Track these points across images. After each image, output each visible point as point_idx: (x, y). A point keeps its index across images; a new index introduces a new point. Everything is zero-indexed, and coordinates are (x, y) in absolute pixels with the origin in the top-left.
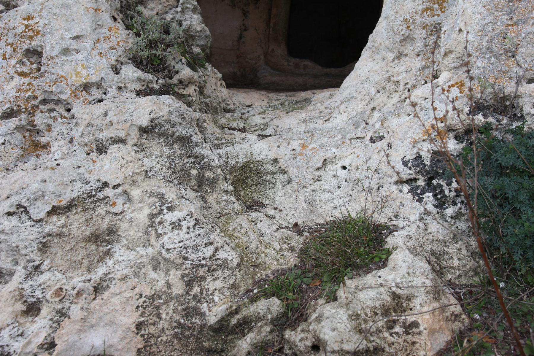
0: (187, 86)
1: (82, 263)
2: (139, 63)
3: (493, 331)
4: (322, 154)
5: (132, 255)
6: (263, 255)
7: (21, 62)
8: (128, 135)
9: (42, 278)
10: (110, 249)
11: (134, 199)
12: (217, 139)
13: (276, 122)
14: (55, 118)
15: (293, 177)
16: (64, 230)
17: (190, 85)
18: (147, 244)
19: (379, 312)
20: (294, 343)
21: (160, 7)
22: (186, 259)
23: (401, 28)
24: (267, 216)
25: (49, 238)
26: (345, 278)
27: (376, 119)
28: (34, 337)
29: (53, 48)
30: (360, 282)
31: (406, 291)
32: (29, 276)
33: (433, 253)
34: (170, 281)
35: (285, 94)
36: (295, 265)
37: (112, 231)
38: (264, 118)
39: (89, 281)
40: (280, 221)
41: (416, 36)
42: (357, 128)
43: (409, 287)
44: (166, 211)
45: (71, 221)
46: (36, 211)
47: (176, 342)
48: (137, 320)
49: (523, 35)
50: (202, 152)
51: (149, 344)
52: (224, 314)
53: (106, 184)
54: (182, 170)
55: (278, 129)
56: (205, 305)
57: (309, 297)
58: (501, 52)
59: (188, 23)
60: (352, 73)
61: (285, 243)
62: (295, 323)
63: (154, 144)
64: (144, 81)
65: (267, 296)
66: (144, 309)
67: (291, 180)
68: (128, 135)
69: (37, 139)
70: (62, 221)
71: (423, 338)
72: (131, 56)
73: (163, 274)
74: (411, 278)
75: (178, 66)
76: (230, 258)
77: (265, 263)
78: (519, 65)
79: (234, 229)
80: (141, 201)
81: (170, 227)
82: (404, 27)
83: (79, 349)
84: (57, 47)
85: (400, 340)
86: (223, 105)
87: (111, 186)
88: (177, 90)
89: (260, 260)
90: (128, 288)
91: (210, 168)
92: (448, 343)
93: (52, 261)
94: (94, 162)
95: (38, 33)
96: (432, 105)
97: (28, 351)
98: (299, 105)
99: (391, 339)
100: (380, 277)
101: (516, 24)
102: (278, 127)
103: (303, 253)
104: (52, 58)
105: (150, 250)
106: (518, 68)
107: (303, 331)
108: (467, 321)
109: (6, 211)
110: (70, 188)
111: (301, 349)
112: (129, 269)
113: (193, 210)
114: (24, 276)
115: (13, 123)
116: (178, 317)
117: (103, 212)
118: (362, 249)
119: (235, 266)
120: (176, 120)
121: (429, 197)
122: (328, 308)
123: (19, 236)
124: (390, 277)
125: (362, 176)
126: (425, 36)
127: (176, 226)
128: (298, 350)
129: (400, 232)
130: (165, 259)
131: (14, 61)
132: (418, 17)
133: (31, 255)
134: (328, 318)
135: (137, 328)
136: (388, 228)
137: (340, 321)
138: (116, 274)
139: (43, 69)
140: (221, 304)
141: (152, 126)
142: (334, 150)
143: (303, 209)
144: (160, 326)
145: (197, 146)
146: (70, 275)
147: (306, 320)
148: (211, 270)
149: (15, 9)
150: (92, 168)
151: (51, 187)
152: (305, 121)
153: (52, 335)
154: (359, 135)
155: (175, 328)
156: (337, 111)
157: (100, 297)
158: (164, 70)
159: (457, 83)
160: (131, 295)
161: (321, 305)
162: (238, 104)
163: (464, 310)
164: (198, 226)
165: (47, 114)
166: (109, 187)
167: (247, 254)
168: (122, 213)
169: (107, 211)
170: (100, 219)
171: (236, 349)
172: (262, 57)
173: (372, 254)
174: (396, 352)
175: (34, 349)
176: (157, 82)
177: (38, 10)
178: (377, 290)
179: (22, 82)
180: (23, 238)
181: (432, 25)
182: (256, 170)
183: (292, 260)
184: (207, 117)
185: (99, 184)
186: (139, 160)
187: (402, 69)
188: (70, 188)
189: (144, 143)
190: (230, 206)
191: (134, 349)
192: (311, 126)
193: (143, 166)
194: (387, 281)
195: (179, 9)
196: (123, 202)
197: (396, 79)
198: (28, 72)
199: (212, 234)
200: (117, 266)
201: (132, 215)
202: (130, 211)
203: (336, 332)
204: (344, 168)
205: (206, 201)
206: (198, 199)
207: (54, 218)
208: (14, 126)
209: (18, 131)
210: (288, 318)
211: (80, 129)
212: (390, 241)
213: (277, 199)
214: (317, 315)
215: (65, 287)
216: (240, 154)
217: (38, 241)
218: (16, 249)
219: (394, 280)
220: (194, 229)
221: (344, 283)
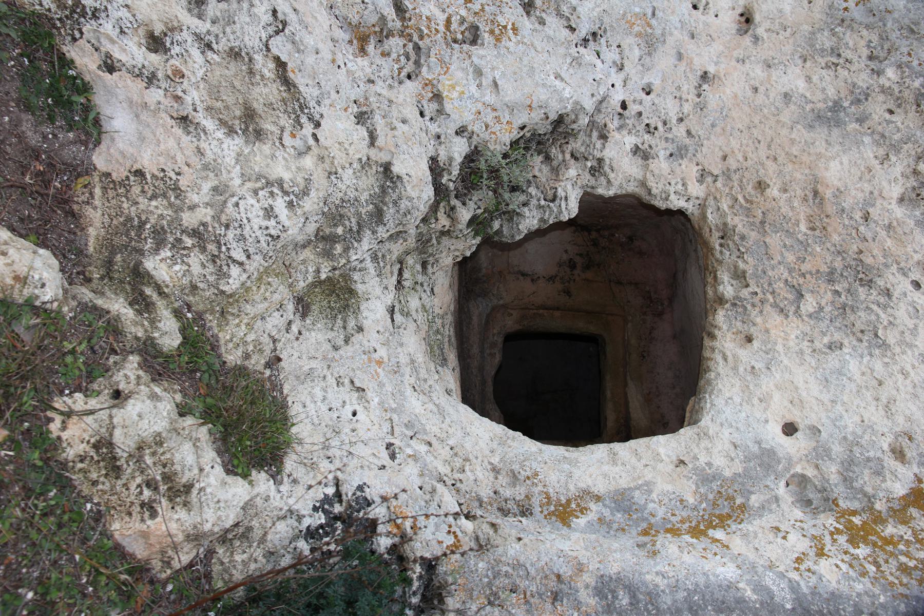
0: (449, 216)
1: (217, 100)
2: (471, 158)
3: (152, 608)
4: (370, 386)
5: (230, 160)
6: (237, 321)
7: (463, 21)
8: (381, 149)
9: (195, 53)
10: (236, 133)
11: (301, 160)
12: (383, 256)
13: (412, 326)
14: (398, 61)
15: (341, 352)
16: (258, 77)
17: (449, 219)
18: (245, 178)
19: (166, 470)
20: (123, 368)
21: (544, 180)
22: (227, 227)
23: (528, 469)
24: (290, 323)
25: (246, 59)
26: (210, 425)
27: (417, 448)
28: (120, 47)
29: (482, 57)
30: (204, 444)
31: (195, 500)
32: (198, 37)
33: (249, 529)
34: (198, 209)
35: (452, 333)
36: (225, 362)
37: (259, 134)
38: (417, 311)
39: (195, 110)
40: (283, 339)
41: (518, 488)
42: (406, 425)
43: (201, 503)
44: (287, 199)
45: (270, 85)
46: (280, 44)
47: (121, 220)
48: (146, 170)
49: (513, 611)
50: (365, 239)
51: (118, 187)
52: (157, 279)
53: (318, 125)
54: (341, 215)
55: (401, 330)
56: (169, 254)
57: (184, 382)
58: (494, 589)
59: (527, 214)
60: (477, 415)
61: (255, 347)
62: (149, 367)
63: (372, 180)
64: (450, 165)
65: (183, 330)
66: (162, 179)
67: (337, 350)
68: (381, 149)
69: (372, 40)
70: (268, 74)
71: (137, 524)
72: (479, 149)
73: (206, 200)
74: (212, 505)
75: (471, 205)
76: (231, 281)
77: (227, 325)
78: (479, 610)
79: (269, 284)
80: (299, 168)
81: (266, 206)
82: (529, 473)
83: (108, 101)
84: (483, 63)
85: (133, 497)
86: (431, 260)
87: (315, 131)
88: (442, 205)
89: (230, 318)
90: (188, 157)
91: (346, 250)
92: (133, 556)
93: (218, 64)
94: (346, 110)
95: (498, 40)
96: (432, 514)
97: (102, 40)
98: (437, 352)
99: (133, 486)
100: (212, 467)
101: (527, 602)
102: (405, 329)
103: (241, 371)
104: (470, 57)
105: (237, 182)
106: (476, 609)
107: (139, 377)
108: (164, 576)
109: (277, 8)
110: (310, 83)
111: (115, 377)
112: (213, 157)
113: (290, 232)
114: (198, 31)
115: (390, 12)
116: (153, 221)
117: (282, 122)
118: (248, 443)
119: (221, 288)
120: (403, 206)
121: (320, 519)
122: (168, 407)
123: (248, 24)
124: (212, 480)
125: (343, 437)
126: (517, 498)
127: (269, 213)
128: (114, 374)
129: (273, 487)
130: (225, 202)
131: (463, 12)
132: (540, 488)
133: (224, 40)
134: (155, 408)
135: (136, 171)
136: (279, 472)
137: (152, 423)
138: (205, 141)
139: (456, 46)
140: (171, 274)
141: (392, 178)
142: (376, 400)
143: (301, 367)
144: (140, 199)
145: (373, 233)
146: (202, 86)
147: (153, 380)
148: (214, 259)
149: (524, 14)
150: (338, 107)
151: (310, 60)
152: (413, 362)
153: (124, 69)
154: (396, 428)
155: (139, 218)
156: (427, 401)
157: (174, 124)
158: (466, 188)
159: (459, 541)
160: (179, 161)
161: (174, 398)
162: (434, 278)
163: (177, 571)
164: (270, 239)
165: (402, 51)
166: (314, 128)
167: (237, 301)
168: (283, 145)
169: (284, 127)
170: (273, 120)
171: (113, 296)
172: (501, 302)
173: (243, 455)
174: (116, 494)
175: (104, 47)
176: (450, 180)
177: (525, 40)
178: (195, 465)
179: (439, 22)
180: (245, 30)
181: (530, 505)
182: (348, 306)
183: (233, 358)
184: (411, 242)
185: (317, 117)
186: (351, 164)
187: (480, 475)
188: (310, 83)
189: (371, 168)
190: (300, 277)
191: (110, 168)
192: (408, 370)
193: (343, 168)
194: (207, 476)
195: (543, 202)
196: (297, 146)
197: (467, 468)
198: (452, 29)
199: (262, 257)
200: (215, 142)
201: (280, 158)
202: (286, 155)
203: (137, 418)
204: (354, 414)
205: (304, 247)
206: (306, 237)
207: (272, 65)
208: (385, 14)
209: (380, 18)
210: (155, 357)
211: (384, 92)
212: (261, 479)
213: (313, 334)
214: (159, 393)
215: (185, 81)
216: (367, 285)
217: (242, 46)
218: (231, 20)
219: (209, 485)
220: (266, 235)
221: (203, 424)
